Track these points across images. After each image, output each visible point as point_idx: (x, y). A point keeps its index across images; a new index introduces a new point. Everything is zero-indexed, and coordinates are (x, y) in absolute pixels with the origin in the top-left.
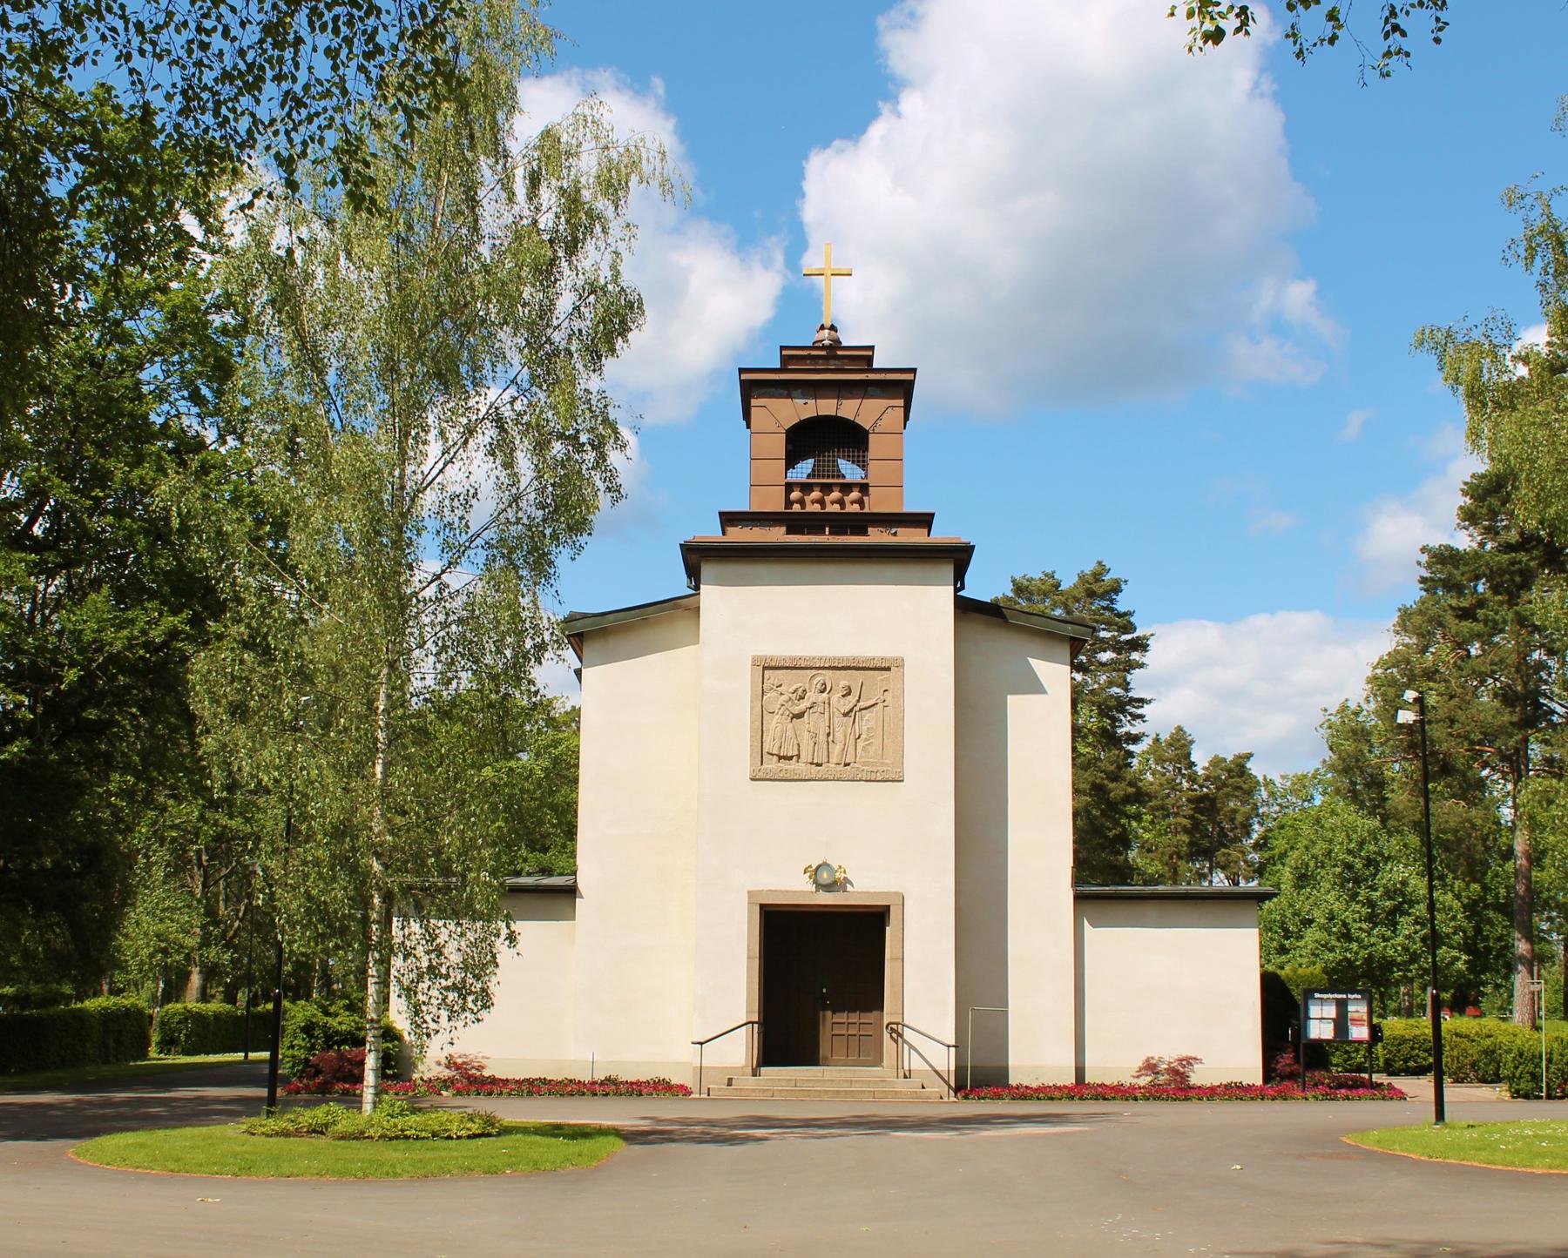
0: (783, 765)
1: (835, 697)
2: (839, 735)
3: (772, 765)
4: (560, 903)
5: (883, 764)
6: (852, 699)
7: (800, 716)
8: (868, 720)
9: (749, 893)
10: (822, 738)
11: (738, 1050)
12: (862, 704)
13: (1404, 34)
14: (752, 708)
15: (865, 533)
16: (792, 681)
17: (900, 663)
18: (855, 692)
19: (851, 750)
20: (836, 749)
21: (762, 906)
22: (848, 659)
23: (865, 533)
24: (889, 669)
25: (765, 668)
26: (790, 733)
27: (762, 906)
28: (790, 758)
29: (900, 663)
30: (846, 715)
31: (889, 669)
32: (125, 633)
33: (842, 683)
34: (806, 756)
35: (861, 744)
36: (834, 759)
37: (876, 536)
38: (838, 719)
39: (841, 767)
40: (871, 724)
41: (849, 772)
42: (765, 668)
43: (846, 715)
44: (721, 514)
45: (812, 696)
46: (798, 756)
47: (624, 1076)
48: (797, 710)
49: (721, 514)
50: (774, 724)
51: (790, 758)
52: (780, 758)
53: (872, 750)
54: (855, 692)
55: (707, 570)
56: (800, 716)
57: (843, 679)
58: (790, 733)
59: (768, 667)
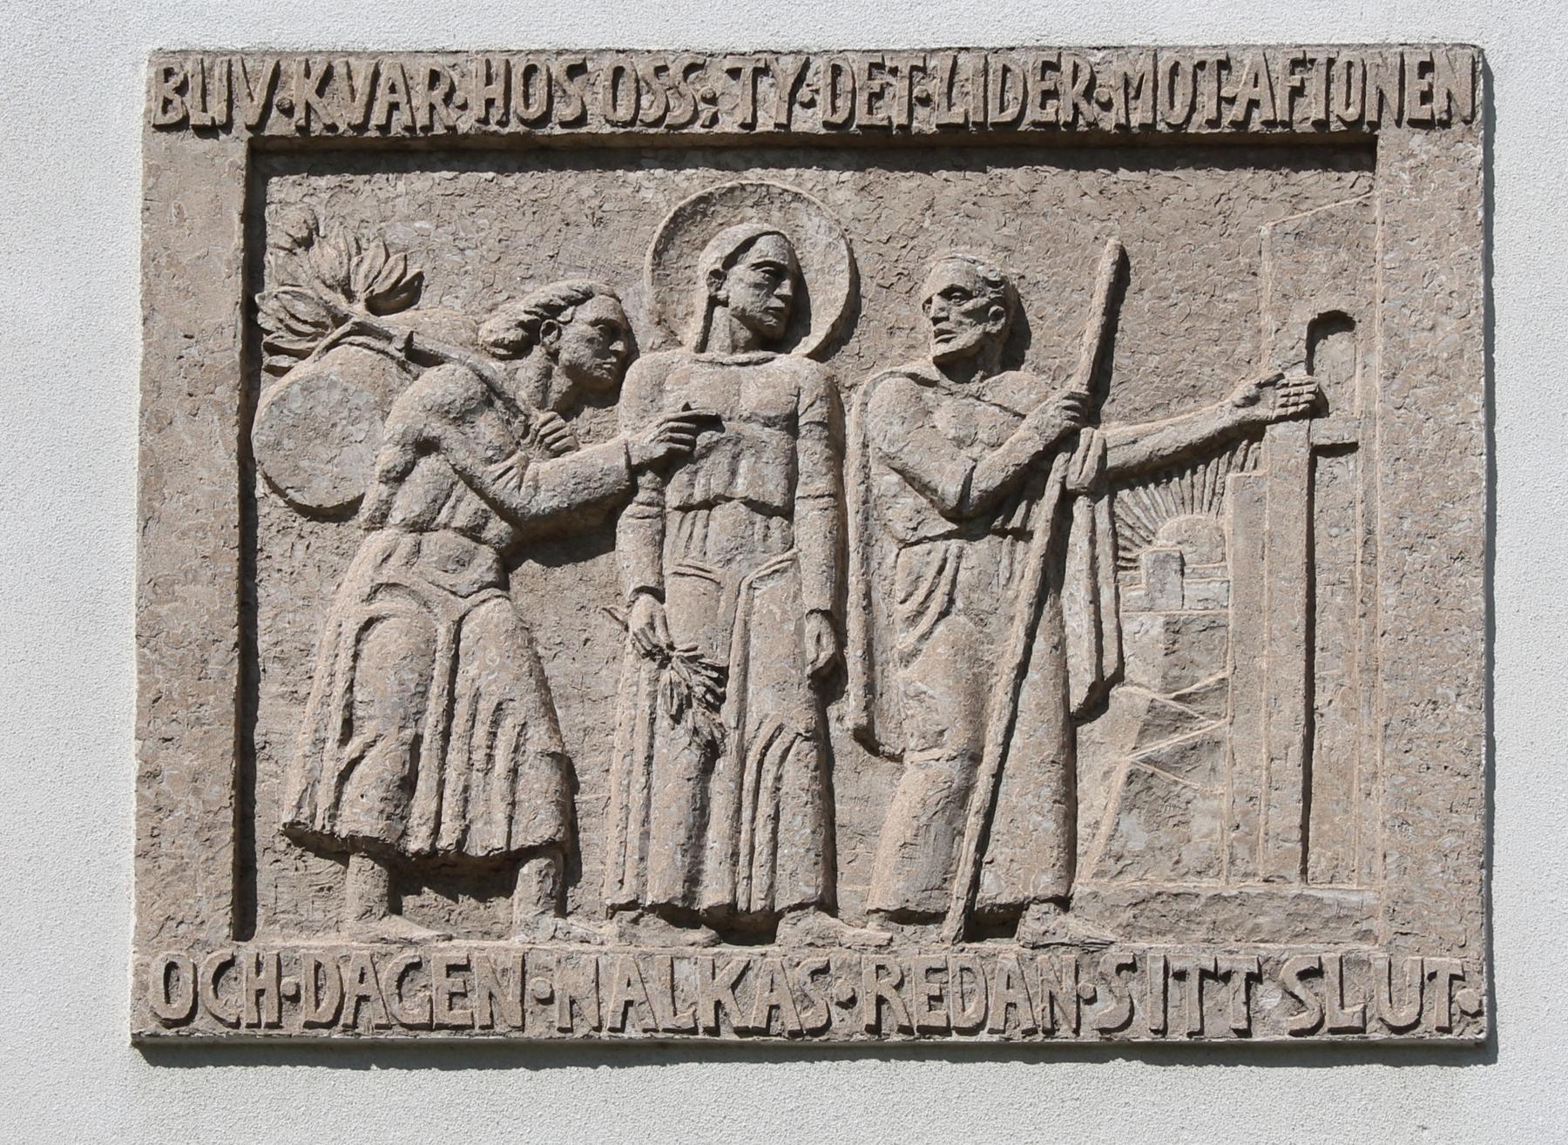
0: (428, 928)
2: (920, 684)
3: (331, 927)
5: (1304, 919)
6: (1030, 399)
7: (576, 533)
8: (1196, 557)
10: (771, 703)
12: (1121, 436)
14: (155, 475)
16: (483, 254)
17: (1453, 99)
18: (1065, 340)
19: (1027, 799)
20: (893, 807)
22: (996, 67)
24: (1350, 148)
25: (268, 158)
26: (489, 669)
28: (491, 877)
29: (1453, 99)
30: (980, 515)
32: (695, 704)
35: (1108, 754)
36: (879, 876)
38: (906, 561)
40: (1197, 594)
41: (998, 980)
42: (268, 158)
43: (980, 515)
44: (185, 101)
45: (675, 374)
46: (564, 857)
48: (547, 484)
49: (185, 101)
50: (328, 599)
51: (491, 877)
53: (1209, 804)
54: (1065, 340)
55: (465, 962)
56: (576, 533)
57: (953, 230)
58: (489, 669)
59: (290, 137)
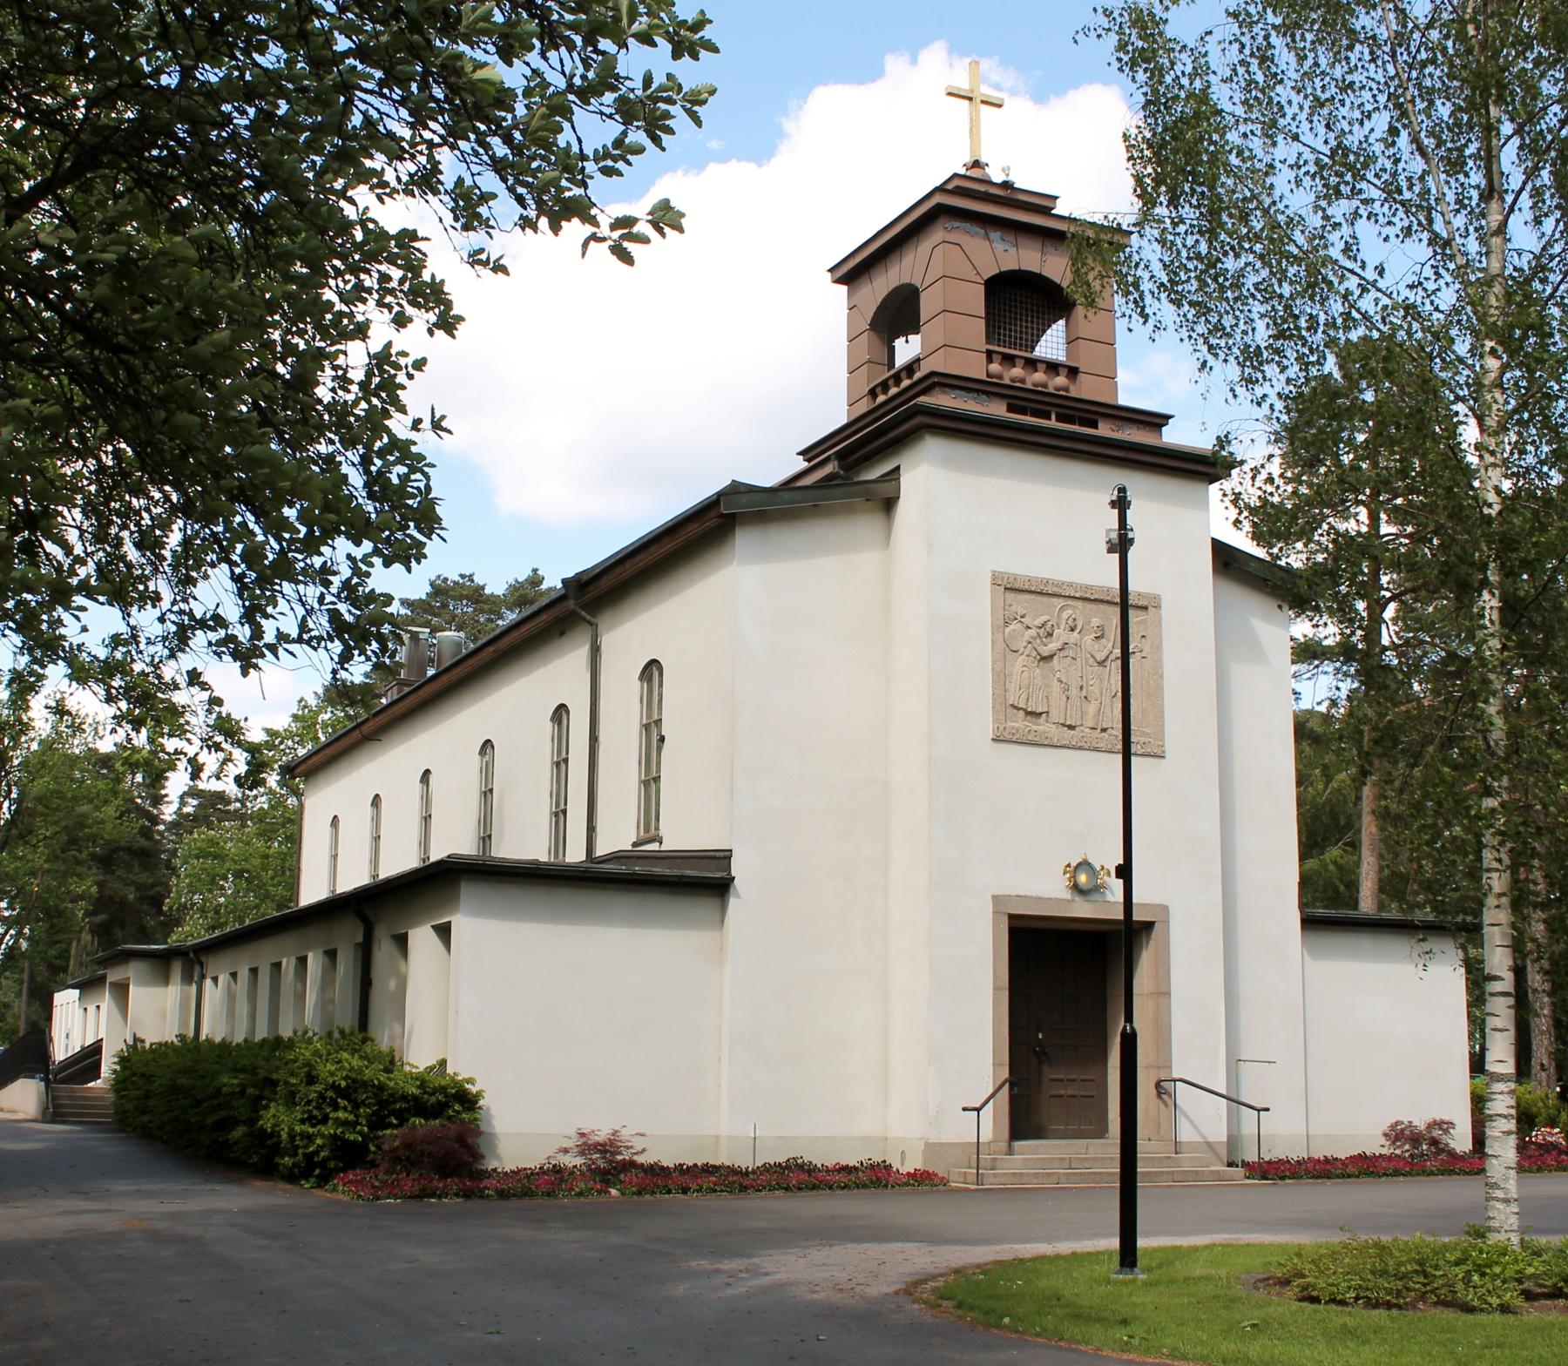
1: (1088, 639)
3: (1019, 723)
4: (702, 907)
9: (994, 897)
11: (992, 1124)
13: (448, 323)
15: (1096, 427)
16: (1037, 612)
21: (1012, 917)
23: (1096, 427)
24: (1146, 608)
27: (1012, 917)
31: (1146, 608)
33: (1096, 621)
34: (1056, 716)
37: (1104, 430)
39: (1097, 734)
45: (1061, 635)
47: (821, 1157)
48: (1045, 651)
52: (1028, 713)
59: (1010, 587)
